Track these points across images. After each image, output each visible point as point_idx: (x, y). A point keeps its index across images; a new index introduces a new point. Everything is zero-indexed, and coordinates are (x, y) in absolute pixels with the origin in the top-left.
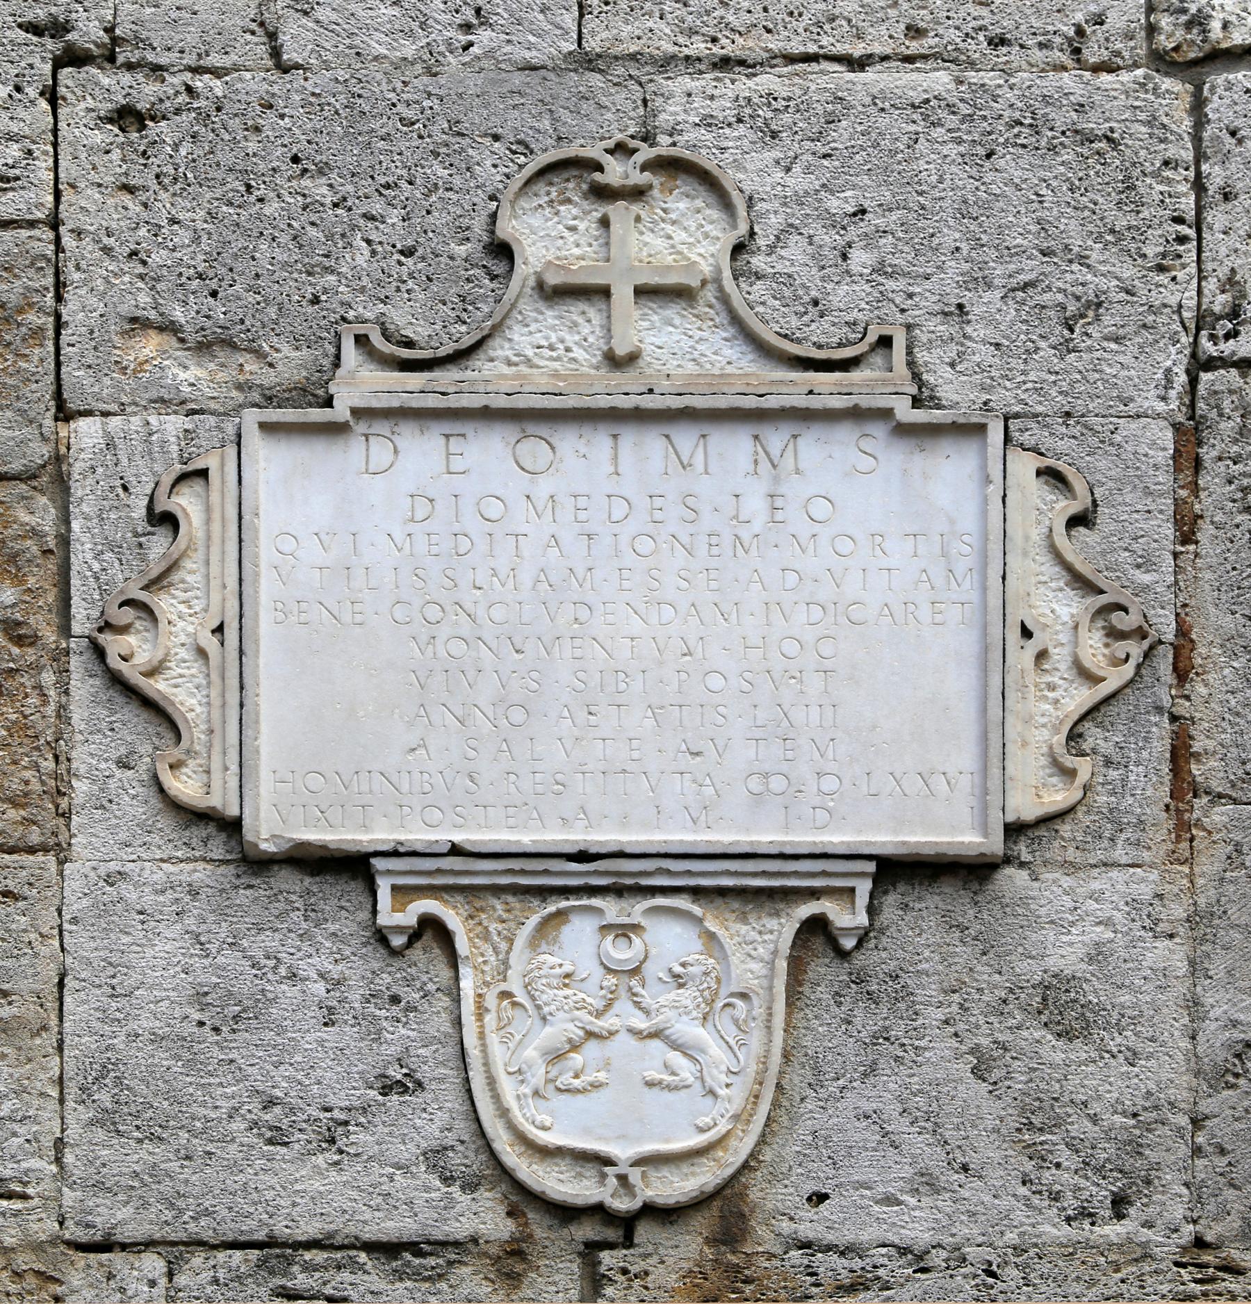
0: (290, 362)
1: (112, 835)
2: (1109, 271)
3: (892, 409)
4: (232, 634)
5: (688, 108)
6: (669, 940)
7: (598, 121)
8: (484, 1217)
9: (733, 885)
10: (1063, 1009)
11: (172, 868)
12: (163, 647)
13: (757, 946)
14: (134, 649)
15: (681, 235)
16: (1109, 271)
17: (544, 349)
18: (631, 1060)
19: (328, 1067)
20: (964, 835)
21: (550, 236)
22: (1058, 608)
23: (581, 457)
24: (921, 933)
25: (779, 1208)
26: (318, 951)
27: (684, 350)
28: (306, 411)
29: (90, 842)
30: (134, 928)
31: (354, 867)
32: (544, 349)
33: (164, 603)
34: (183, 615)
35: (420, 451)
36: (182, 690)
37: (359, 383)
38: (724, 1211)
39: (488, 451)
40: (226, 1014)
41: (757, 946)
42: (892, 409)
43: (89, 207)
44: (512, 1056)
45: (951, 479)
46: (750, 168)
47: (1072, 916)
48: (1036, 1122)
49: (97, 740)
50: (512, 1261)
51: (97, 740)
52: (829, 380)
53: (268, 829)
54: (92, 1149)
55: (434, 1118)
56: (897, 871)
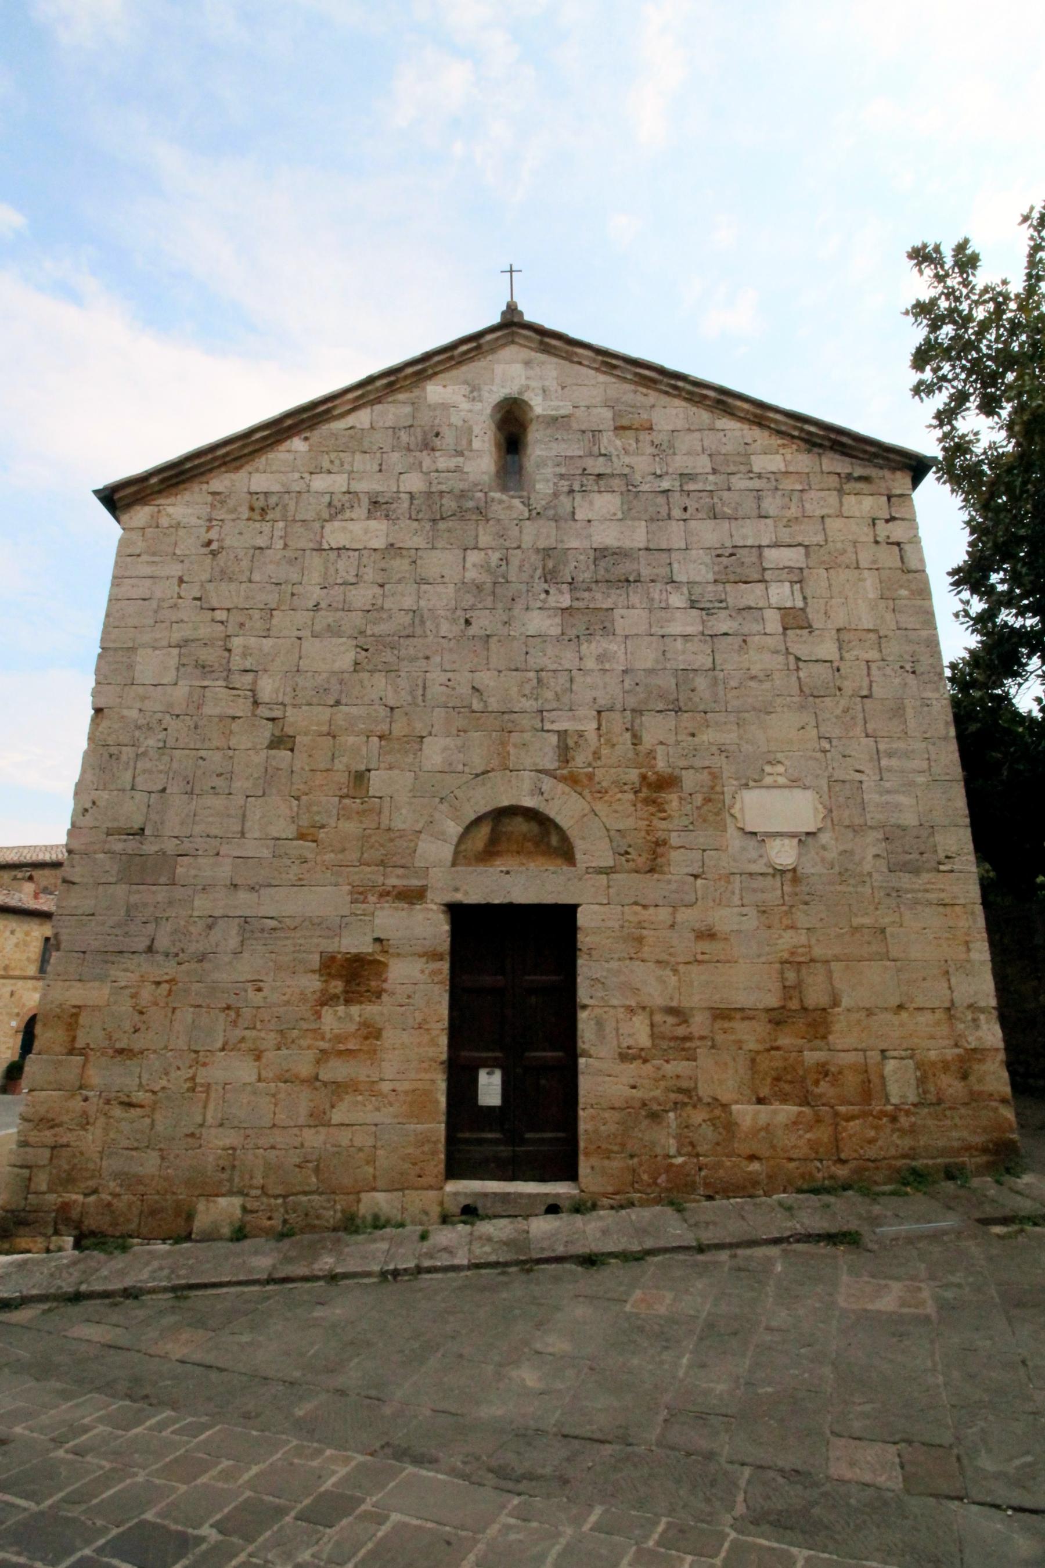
0: (744, 781)
1: (731, 830)
2: (819, 772)
3: (571, 910)
4: (742, 809)
5: (780, 756)
6: (787, 841)
7: (771, 757)
8: (771, 871)
9: (792, 835)
10: (824, 848)
11: (737, 834)
12: (735, 811)
13: (795, 841)
14: (732, 811)
15: (780, 769)
16: (819, 772)
17: (768, 780)
18: (784, 854)
19: (754, 855)
20: (814, 830)
21: (768, 769)
22: (820, 806)
23: (775, 791)
24: (810, 839)
25: (800, 870)
26: (752, 843)
27: (782, 780)
28: (746, 785)
29: (729, 830)
30: (734, 841)
31: (755, 834)
32: (768, 780)
33: (711, 1227)
34: (738, 806)
35: (757, 792)
36: (738, 815)
37: (751, 784)
38: (794, 870)
39: (764, 791)
40: (744, 849)
41: (795, 841)
42: (571, 910)
43: (724, 766)
44: (772, 854)
45: (809, 794)
46: (786, 762)
47: (825, 838)
48: (823, 860)
49: (729, 820)
50: (774, 876)
51: (729, 820)
52: (795, 783)
53: (748, 829)
54: (732, 863)
55: (764, 861)
56: (808, 834)
